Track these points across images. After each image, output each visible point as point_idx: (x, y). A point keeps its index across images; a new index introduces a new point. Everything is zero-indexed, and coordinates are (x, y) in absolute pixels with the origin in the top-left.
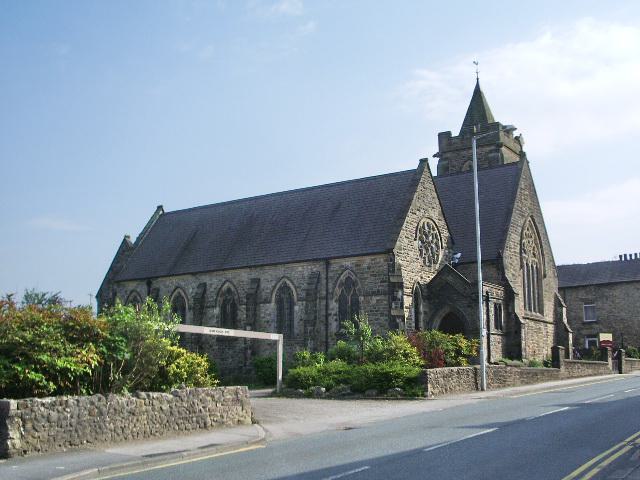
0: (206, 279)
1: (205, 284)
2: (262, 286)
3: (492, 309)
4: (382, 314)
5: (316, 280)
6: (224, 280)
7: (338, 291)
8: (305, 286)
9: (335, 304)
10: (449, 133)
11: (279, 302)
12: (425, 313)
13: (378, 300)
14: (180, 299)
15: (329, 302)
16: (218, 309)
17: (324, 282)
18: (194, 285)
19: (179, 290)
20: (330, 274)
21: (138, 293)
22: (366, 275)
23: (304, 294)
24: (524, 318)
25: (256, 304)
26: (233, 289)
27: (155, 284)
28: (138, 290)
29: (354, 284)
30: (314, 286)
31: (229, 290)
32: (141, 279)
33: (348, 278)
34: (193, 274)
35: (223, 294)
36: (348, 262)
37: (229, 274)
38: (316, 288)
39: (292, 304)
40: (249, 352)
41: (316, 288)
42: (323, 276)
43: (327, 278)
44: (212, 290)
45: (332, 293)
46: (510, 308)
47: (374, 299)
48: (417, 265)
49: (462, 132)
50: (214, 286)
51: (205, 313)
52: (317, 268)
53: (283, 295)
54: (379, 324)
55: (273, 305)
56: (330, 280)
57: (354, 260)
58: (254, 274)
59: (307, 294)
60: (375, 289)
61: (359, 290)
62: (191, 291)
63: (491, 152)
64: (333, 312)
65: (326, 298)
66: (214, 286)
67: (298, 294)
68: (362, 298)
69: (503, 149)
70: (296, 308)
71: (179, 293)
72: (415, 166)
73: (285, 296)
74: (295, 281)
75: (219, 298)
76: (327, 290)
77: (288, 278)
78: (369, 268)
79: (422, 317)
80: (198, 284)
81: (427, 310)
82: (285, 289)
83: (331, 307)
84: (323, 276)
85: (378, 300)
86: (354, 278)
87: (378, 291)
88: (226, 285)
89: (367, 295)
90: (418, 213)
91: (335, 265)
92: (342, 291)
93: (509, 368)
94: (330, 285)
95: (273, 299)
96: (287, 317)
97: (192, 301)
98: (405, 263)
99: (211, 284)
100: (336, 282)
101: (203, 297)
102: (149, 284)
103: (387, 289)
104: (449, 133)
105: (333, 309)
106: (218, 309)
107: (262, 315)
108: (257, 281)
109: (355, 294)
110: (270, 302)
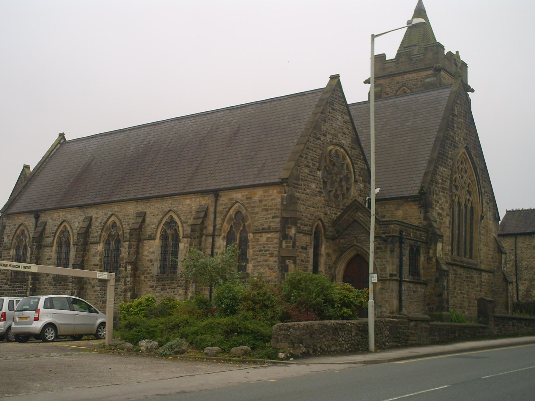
0: (92, 212)
1: (91, 219)
2: (148, 220)
3: (407, 252)
4: (272, 255)
5: (203, 214)
6: (110, 213)
7: (226, 227)
8: (191, 222)
9: (221, 241)
10: (383, 56)
11: (164, 237)
12: (328, 255)
13: (268, 238)
14: (66, 233)
15: (217, 239)
16: (102, 245)
17: (212, 216)
18: (81, 219)
19: (171, 213)
20: (219, 208)
21: (26, 227)
22: (256, 210)
23: (189, 230)
24: (448, 264)
25: (140, 241)
26: (118, 223)
27: (43, 218)
28: (26, 223)
29: (244, 219)
30: (200, 221)
31: (114, 223)
32: (30, 212)
33: (238, 213)
34: (80, 207)
35: (108, 229)
36: (238, 195)
37: (116, 208)
38: (203, 223)
39: (176, 239)
40: (129, 294)
41: (203, 223)
42: (212, 209)
43: (215, 213)
44: (97, 224)
45: (220, 230)
46: (431, 252)
47: (264, 237)
48: (320, 200)
49: (399, 55)
50: (99, 220)
51: (88, 251)
52: (207, 201)
53: (169, 232)
54: (268, 266)
55: (157, 243)
56: (218, 215)
57: (246, 192)
58: (141, 207)
59: (193, 230)
60: (266, 226)
61: (249, 225)
62: (77, 225)
63: (427, 77)
64: (219, 251)
65: (213, 236)
66: (99, 220)
67: (183, 231)
68: (251, 236)
69: (442, 73)
70: (181, 246)
71: (172, 217)
72: (323, 83)
73: (63, 239)
74: (181, 216)
75: (104, 234)
76: (215, 226)
77: (175, 212)
78: (260, 201)
79: (322, 260)
80: (84, 217)
81: (330, 252)
82: (171, 223)
83: (217, 244)
84: (212, 209)
85: (268, 238)
86: (244, 212)
87: (269, 227)
88: (112, 219)
89: (257, 232)
90: (322, 138)
91: (224, 199)
92: (231, 226)
93: (412, 324)
94: (219, 221)
95: (158, 235)
96: (407, 225)
97: (76, 237)
98: (303, 196)
99: (97, 218)
100: (225, 216)
101: (141, 227)
102: (37, 218)
103: (279, 225)
104: (383, 56)
105: (219, 248)
106: (102, 245)
107: (146, 253)
108: (143, 216)
109: (244, 230)
110: (155, 239)
